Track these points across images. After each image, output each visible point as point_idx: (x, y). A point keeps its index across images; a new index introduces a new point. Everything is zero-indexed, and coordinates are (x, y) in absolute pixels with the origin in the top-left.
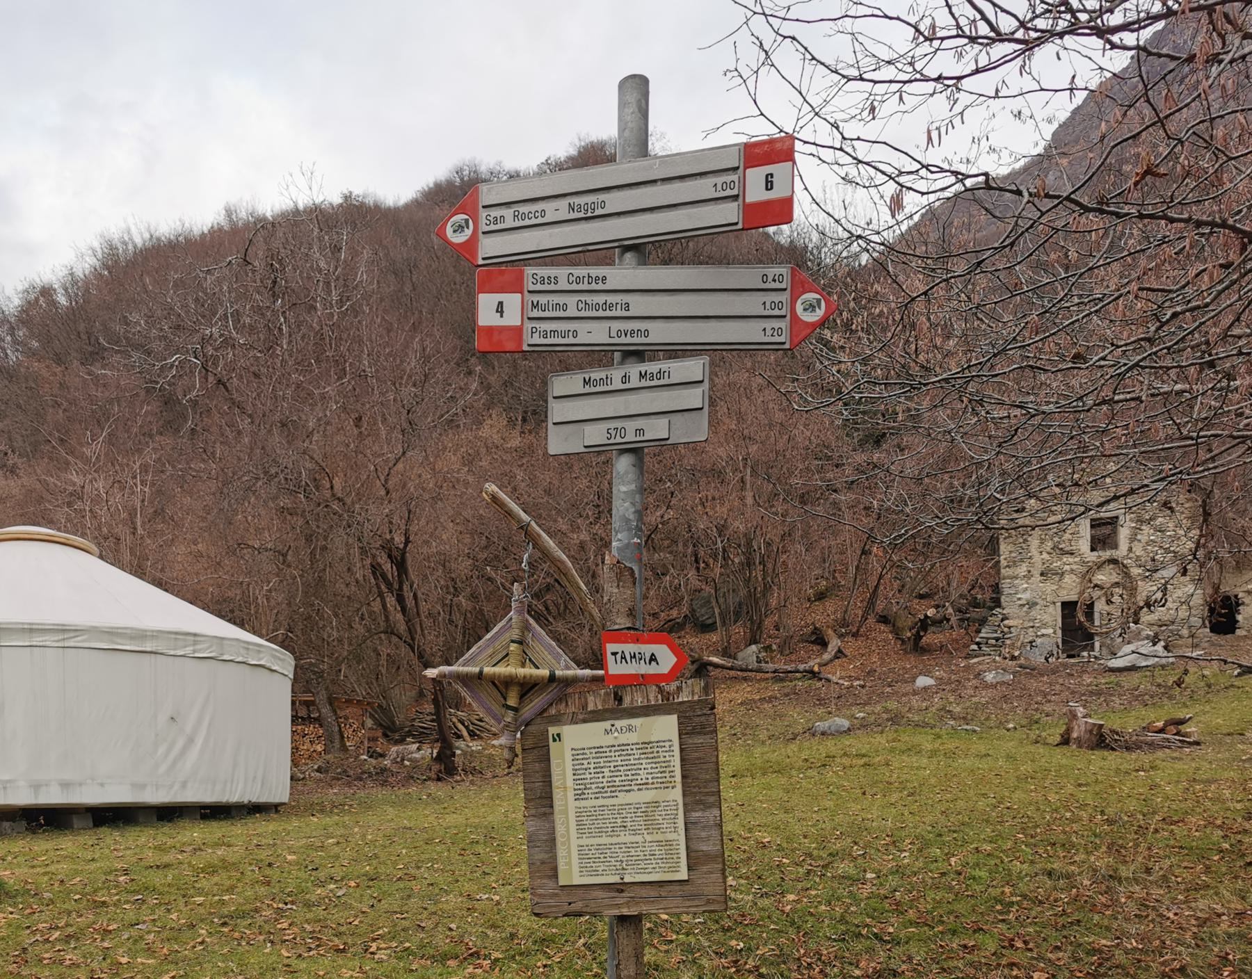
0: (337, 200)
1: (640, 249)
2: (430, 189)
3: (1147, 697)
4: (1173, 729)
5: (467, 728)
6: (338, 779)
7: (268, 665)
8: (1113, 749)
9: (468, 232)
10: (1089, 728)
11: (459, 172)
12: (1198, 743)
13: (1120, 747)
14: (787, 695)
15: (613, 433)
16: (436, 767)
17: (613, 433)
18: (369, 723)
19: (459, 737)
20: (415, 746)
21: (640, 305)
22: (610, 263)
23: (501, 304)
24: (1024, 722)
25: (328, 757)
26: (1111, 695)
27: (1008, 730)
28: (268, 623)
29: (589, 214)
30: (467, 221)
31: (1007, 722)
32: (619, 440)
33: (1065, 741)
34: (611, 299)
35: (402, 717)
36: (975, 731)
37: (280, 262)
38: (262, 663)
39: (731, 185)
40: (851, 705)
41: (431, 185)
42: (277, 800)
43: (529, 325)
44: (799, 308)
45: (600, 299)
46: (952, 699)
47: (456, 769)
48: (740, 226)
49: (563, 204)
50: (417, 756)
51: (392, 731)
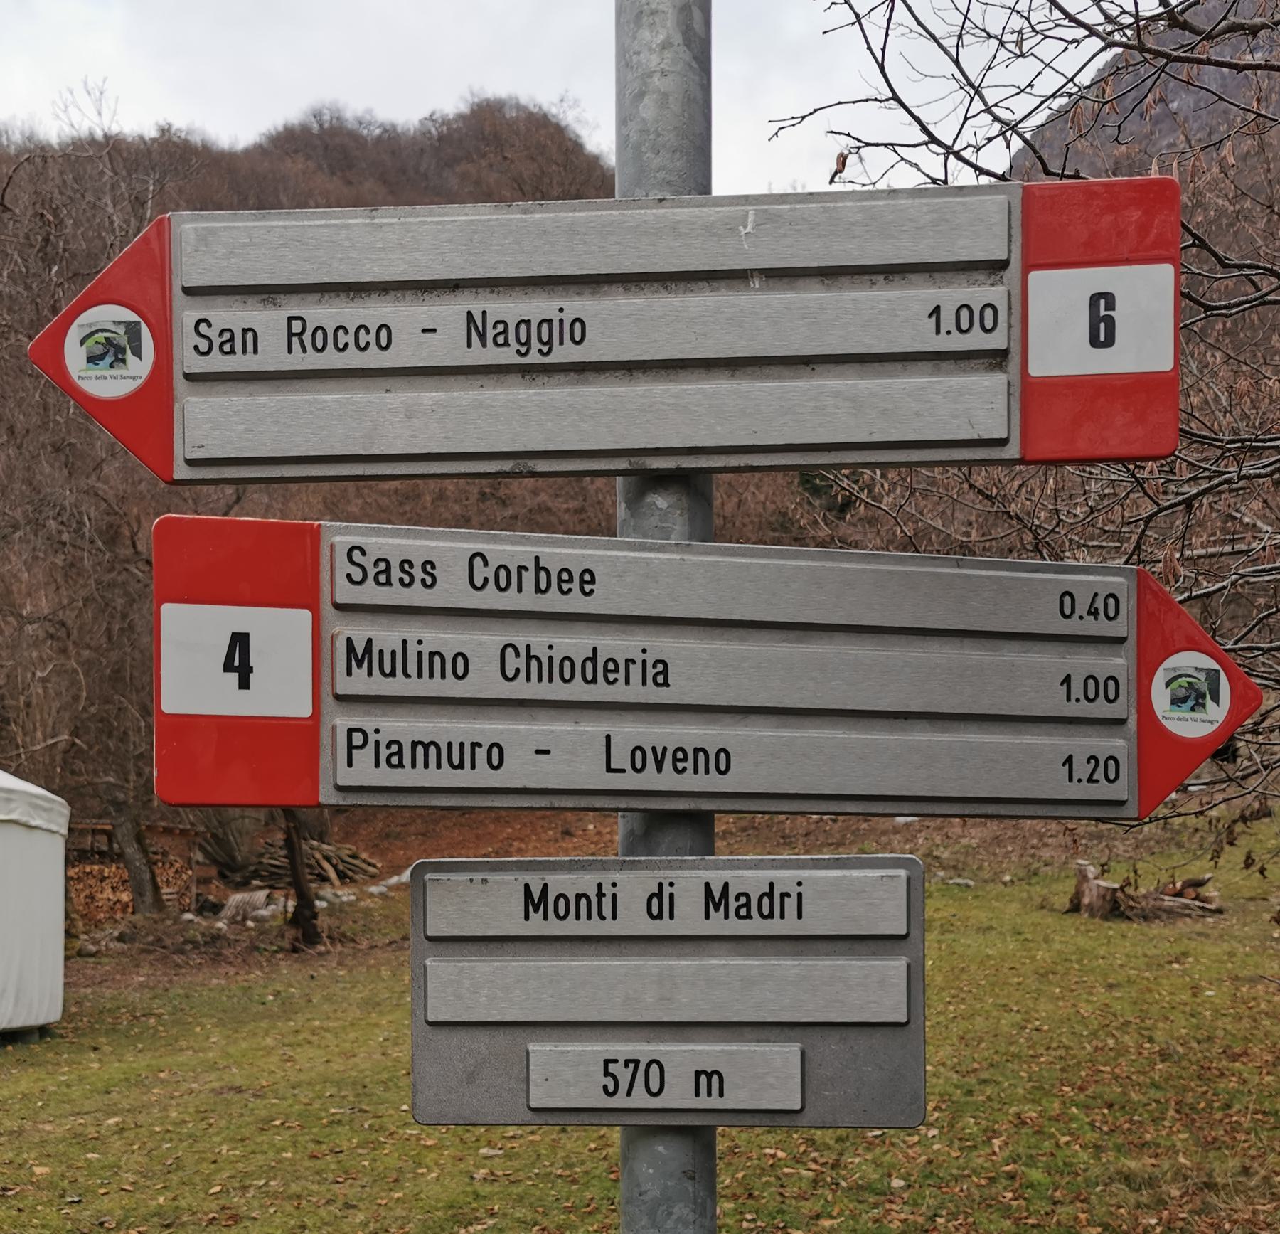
0: (151, 133)
1: (686, 484)
2: (279, 134)
3: (1152, 843)
4: (1191, 892)
5: (335, 867)
6: (149, 952)
7: (24, 819)
8: (1129, 919)
9: (140, 368)
10: (1102, 892)
11: (317, 115)
12: (1219, 911)
13: (1137, 916)
14: (744, 830)
15: (624, 1075)
16: (291, 933)
17: (624, 1075)
18: (199, 856)
19: (324, 879)
20: (261, 895)
21: (699, 668)
22: (599, 525)
23: (240, 641)
24: (1022, 873)
25: (137, 918)
26: (1114, 839)
27: (1005, 884)
28: (44, 726)
29: (534, 358)
30: (132, 331)
31: (1003, 872)
32: (640, 1099)
33: (1075, 907)
34: (614, 644)
35: (245, 849)
36: (968, 886)
37: (55, 212)
38: (13, 816)
39: (982, 318)
40: (822, 845)
41: (281, 129)
42: (41, 1021)
43: (342, 721)
44: (1160, 698)
45: (575, 643)
46: (938, 840)
47: (318, 935)
48: (1012, 451)
49: (449, 313)
50: (264, 913)
51: (234, 872)
